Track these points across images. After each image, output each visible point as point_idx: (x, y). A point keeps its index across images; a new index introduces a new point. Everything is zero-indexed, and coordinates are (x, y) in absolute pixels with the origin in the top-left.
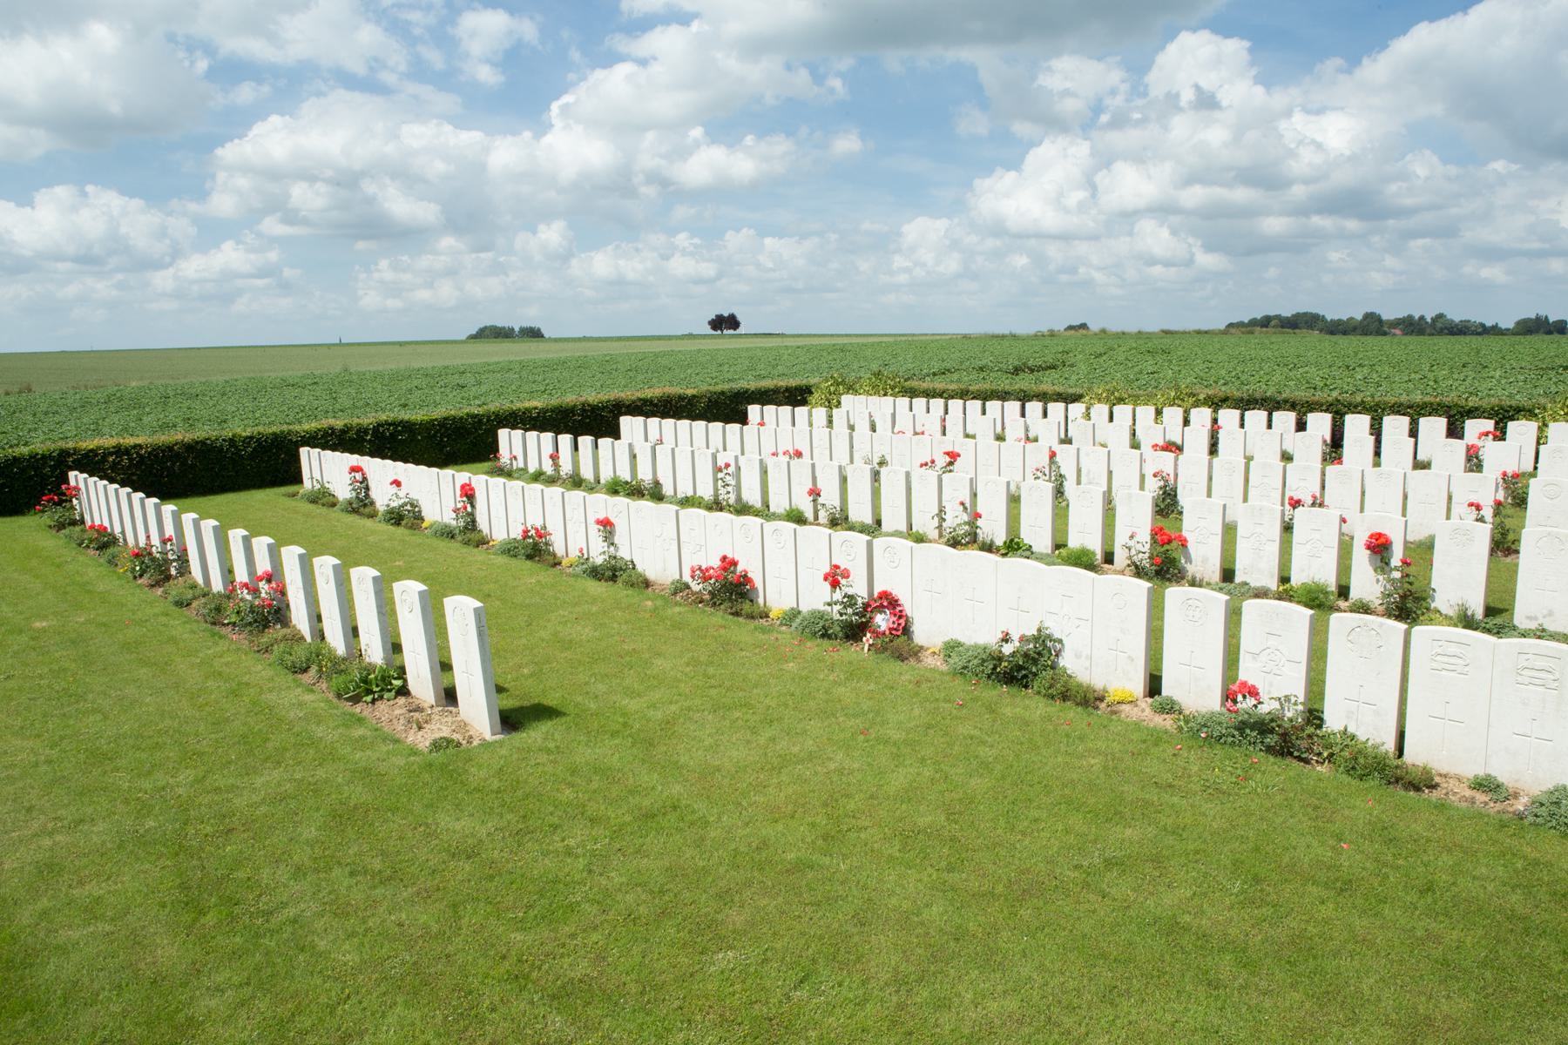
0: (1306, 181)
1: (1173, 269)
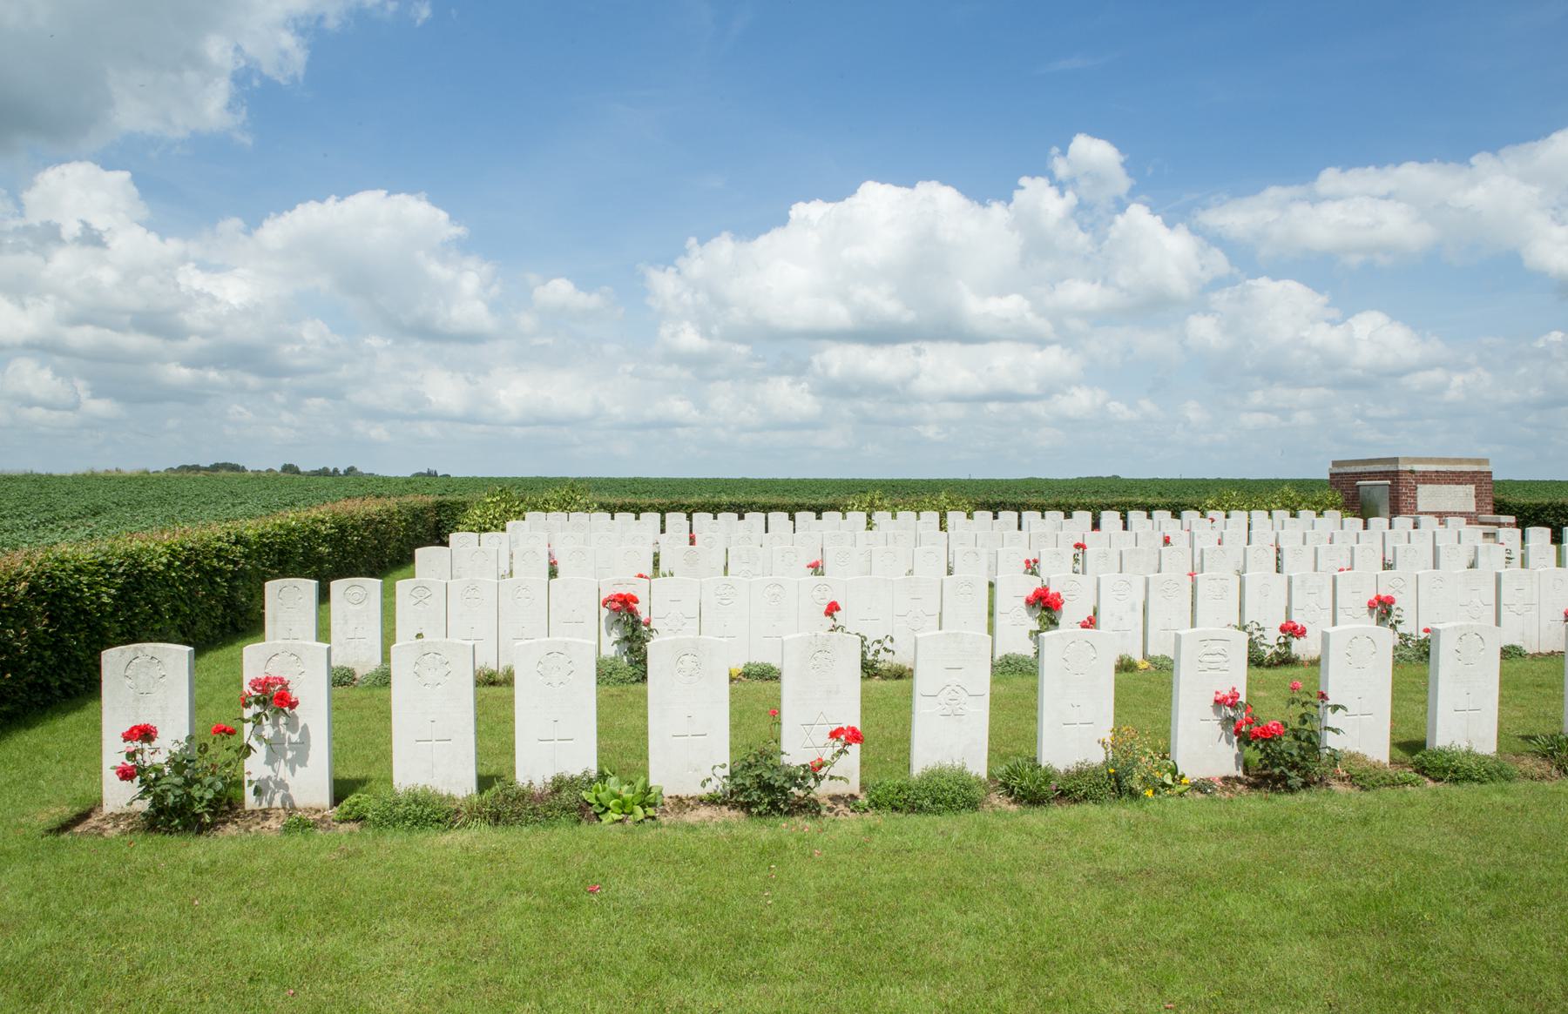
0: (204, 335)
1: (55, 415)
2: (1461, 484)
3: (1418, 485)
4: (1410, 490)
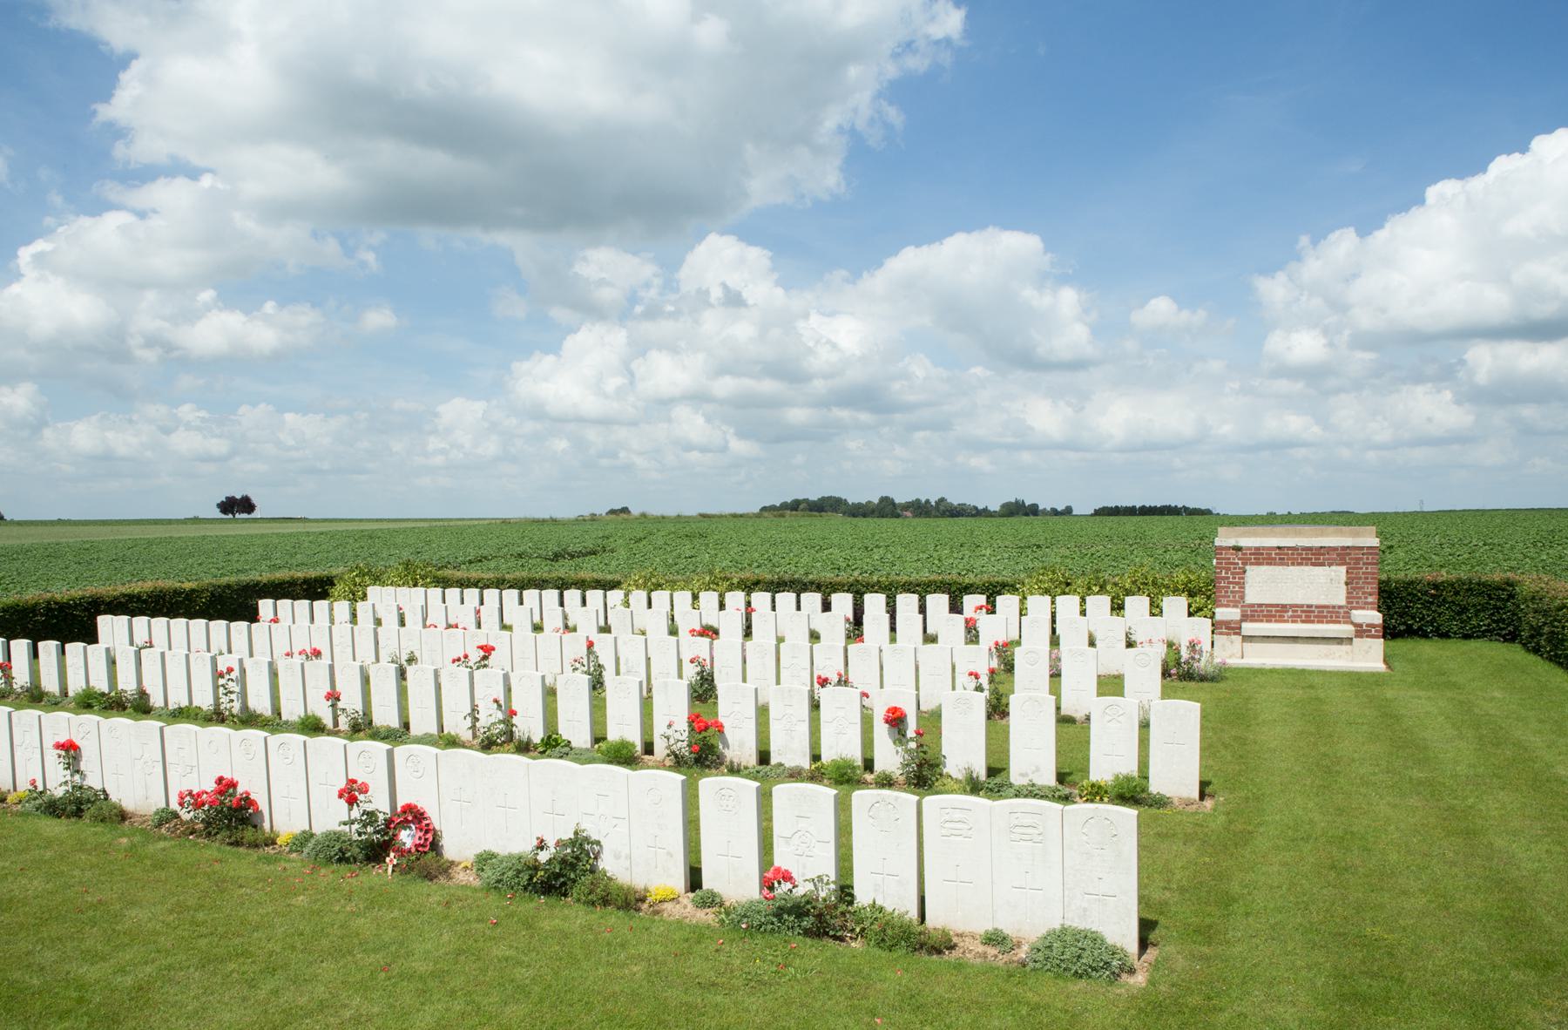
2: (1322, 565)
3: (1248, 567)
4: (1232, 573)
